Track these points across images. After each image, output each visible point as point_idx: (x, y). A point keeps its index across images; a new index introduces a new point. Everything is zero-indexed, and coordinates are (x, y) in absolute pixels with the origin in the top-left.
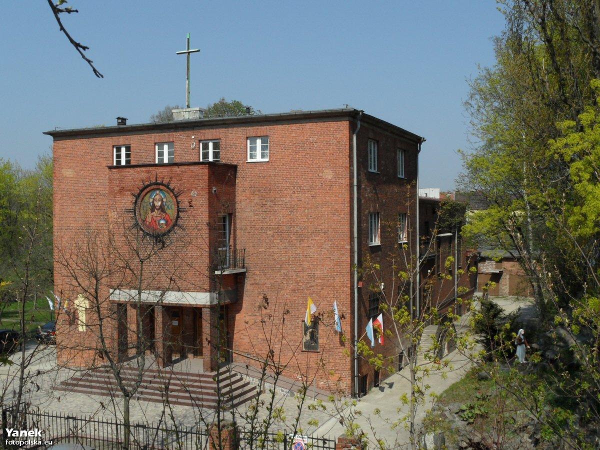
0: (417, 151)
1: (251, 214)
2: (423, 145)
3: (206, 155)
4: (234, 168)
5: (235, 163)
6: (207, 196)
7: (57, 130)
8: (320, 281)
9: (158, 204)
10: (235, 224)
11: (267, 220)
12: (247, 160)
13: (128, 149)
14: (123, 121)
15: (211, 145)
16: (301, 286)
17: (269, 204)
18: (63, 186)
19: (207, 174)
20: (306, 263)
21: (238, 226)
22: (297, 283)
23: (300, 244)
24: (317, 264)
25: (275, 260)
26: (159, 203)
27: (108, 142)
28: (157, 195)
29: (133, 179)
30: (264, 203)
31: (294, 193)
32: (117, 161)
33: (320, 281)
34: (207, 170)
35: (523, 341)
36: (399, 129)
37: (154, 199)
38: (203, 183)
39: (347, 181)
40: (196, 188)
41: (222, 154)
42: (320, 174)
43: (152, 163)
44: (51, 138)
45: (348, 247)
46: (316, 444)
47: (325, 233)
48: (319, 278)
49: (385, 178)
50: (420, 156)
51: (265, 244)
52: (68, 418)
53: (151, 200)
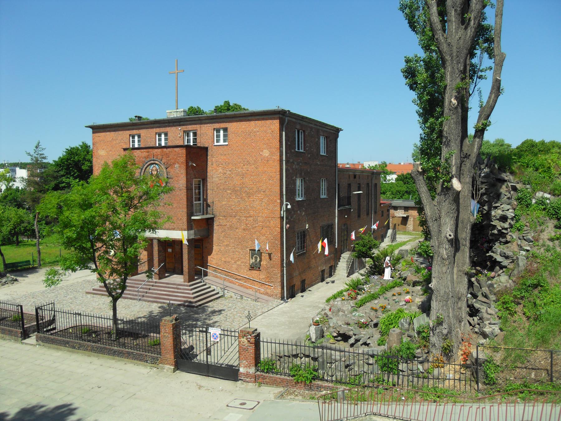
0: (337, 137)
1: (217, 179)
2: (341, 134)
3: (188, 141)
4: (206, 149)
5: (206, 146)
6: (185, 167)
7: (95, 124)
8: (261, 223)
9: (155, 173)
10: (207, 186)
11: (227, 183)
12: (214, 144)
13: (195, 134)
14: (140, 118)
15: (191, 134)
16: (249, 227)
17: (228, 172)
18: (100, 161)
19: (185, 153)
20: (252, 211)
21: (208, 187)
22: (246, 225)
23: (248, 199)
24: (259, 213)
25: (232, 209)
26: (156, 172)
27: (126, 134)
28: (154, 167)
29: (138, 156)
30: (225, 172)
31: (244, 165)
32: (132, 145)
33: (261, 223)
34: (185, 151)
35: (389, 264)
36: (320, 123)
37: (152, 170)
38: (183, 159)
39: (277, 158)
40: (178, 163)
41: (198, 140)
42: (261, 153)
43: (154, 146)
44: (91, 130)
45: (279, 201)
46: (226, 334)
47: (264, 192)
48: (260, 222)
49: (309, 155)
50: (339, 140)
51: (226, 199)
52: (76, 314)
53: (150, 171)
